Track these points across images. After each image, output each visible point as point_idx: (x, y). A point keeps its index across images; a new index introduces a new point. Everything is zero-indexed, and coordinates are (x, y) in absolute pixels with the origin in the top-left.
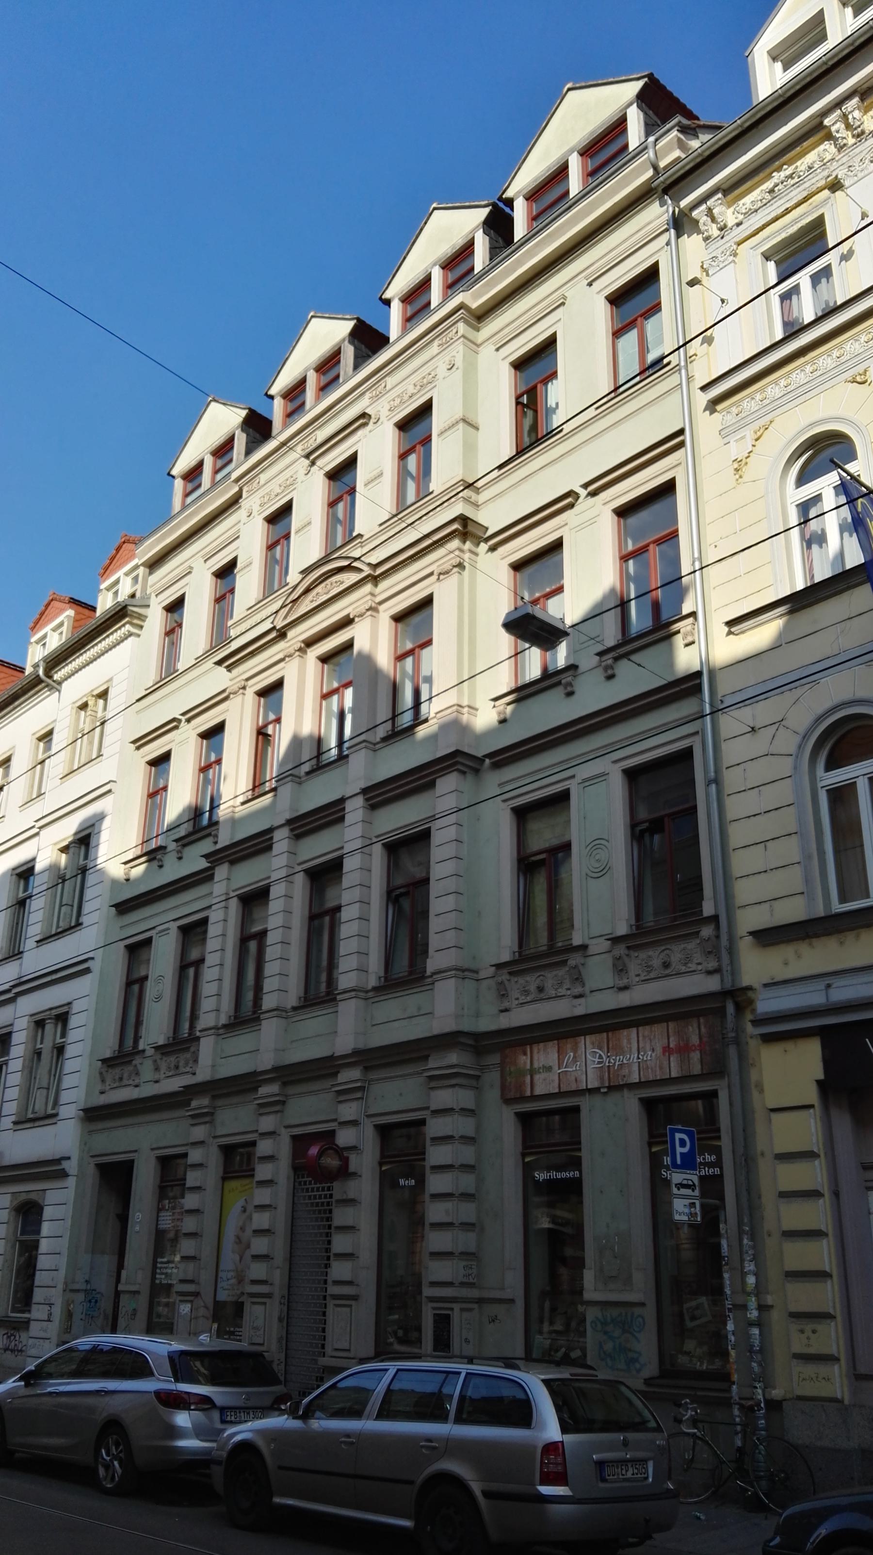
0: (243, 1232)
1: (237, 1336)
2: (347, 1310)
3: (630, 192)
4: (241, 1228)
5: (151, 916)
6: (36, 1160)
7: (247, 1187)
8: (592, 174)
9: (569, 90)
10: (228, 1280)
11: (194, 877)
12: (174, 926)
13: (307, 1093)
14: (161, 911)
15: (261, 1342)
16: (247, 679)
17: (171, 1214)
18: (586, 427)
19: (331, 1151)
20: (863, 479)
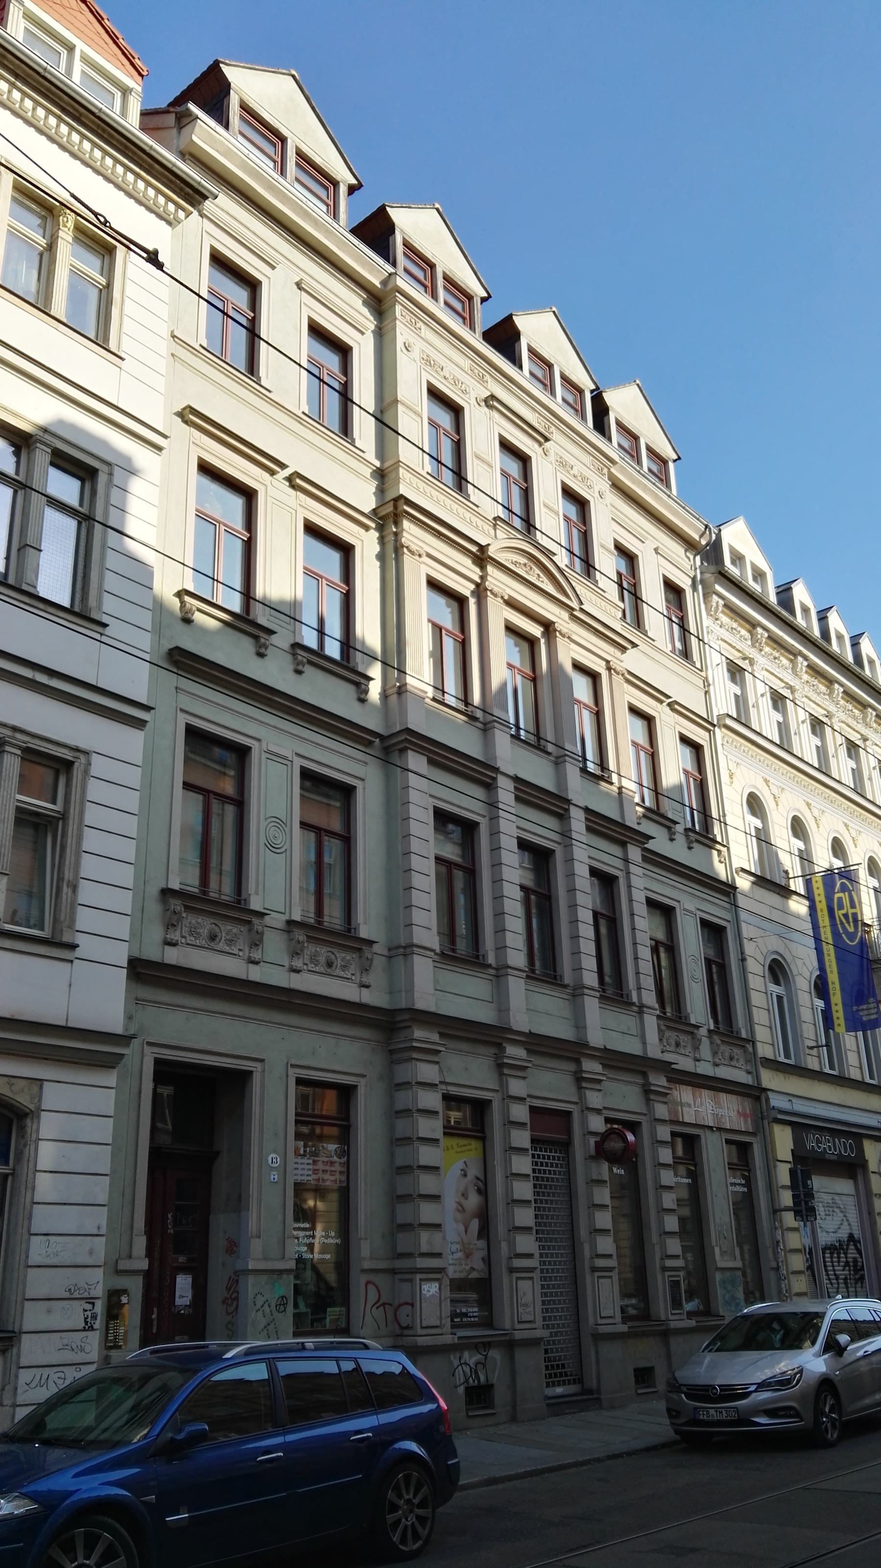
0: (466, 1199)
1: (470, 1317)
2: (609, 1280)
3: (359, 273)
4: (463, 1195)
5: (342, 754)
6: (8, 1016)
7: (464, 1148)
8: (638, 463)
9: (293, 76)
10: (453, 1253)
11: (650, 854)
12: (298, 763)
13: (229, 1015)
14: (272, 724)
15: (532, 1319)
16: (429, 556)
17: (311, 1161)
18: (280, 410)
19: (613, 1136)
20: (727, 818)
